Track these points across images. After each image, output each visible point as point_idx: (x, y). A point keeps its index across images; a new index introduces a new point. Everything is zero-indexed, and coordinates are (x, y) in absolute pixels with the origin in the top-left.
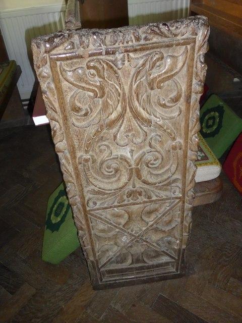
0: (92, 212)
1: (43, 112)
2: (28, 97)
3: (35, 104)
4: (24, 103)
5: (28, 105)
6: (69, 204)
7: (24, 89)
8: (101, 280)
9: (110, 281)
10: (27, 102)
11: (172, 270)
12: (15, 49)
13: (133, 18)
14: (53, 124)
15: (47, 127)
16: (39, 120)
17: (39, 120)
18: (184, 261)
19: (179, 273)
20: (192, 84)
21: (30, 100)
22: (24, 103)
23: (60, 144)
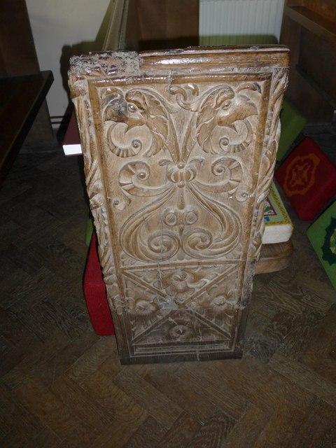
0: (127, 271)
1: (76, 140)
2: (62, 113)
3: (68, 128)
4: (53, 120)
5: (62, 123)
6: (133, 174)
7: (55, 103)
8: (132, 351)
9: (148, 354)
10: (60, 120)
11: (224, 347)
12: (48, 60)
13: (203, 37)
14: (88, 155)
15: (79, 159)
16: (71, 150)
17: (71, 150)
18: (242, 320)
19: (233, 351)
20: (270, 84)
21: (64, 117)
22: (53, 120)
23: (95, 181)
